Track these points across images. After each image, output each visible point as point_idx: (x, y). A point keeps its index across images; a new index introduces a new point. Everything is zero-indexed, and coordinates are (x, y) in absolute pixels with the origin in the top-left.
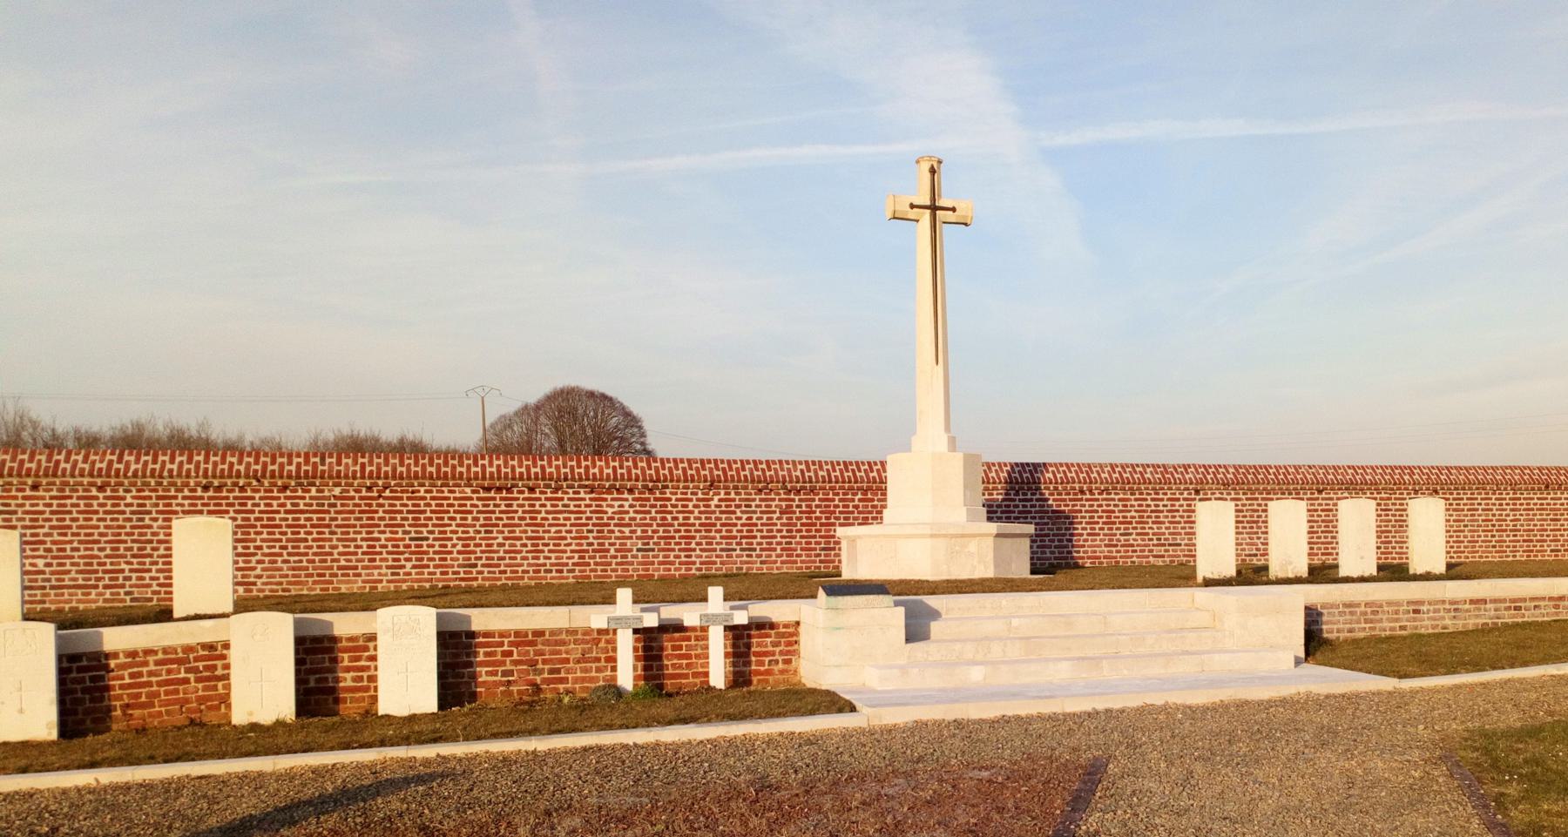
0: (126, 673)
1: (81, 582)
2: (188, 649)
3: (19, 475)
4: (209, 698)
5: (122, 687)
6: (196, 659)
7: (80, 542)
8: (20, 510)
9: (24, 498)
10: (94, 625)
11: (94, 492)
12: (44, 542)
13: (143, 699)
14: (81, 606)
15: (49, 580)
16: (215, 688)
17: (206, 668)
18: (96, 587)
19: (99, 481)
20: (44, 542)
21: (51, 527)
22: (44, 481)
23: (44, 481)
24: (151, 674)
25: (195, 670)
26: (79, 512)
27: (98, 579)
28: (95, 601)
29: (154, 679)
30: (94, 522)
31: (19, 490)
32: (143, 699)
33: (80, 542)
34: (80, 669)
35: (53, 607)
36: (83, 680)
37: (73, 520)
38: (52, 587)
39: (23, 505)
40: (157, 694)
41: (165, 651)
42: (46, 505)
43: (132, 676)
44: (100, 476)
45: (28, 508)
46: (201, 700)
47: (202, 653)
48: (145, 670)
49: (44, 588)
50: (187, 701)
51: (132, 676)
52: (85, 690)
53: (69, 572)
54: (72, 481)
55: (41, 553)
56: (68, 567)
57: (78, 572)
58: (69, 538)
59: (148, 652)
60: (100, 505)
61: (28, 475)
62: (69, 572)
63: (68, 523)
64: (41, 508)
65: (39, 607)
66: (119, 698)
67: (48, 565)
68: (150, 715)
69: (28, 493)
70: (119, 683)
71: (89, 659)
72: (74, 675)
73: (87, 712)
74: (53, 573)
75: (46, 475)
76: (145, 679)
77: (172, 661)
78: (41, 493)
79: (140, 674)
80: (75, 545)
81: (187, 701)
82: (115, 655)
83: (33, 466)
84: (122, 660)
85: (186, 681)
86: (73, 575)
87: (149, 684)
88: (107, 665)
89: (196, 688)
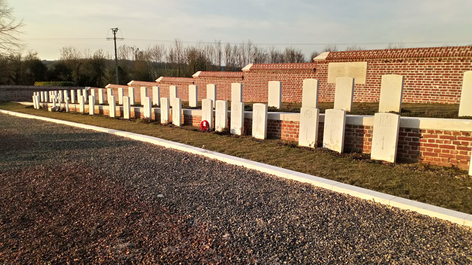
0: (427, 139)
1: (450, 94)
2: (456, 133)
3: (435, 56)
4: (462, 158)
5: (425, 145)
6: (459, 138)
7: (452, 80)
8: (434, 68)
9: (436, 64)
10: (416, 115)
11: (460, 62)
12: (440, 80)
13: (433, 152)
14: (449, 103)
15: (439, 93)
16: (466, 153)
17: (463, 143)
18: (455, 96)
19: (462, 58)
20: (440, 80)
21: (443, 75)
22: (443, 58)
23: (443, 58)
24: (438, 141)
25: (458, 143)
26: (453, 69)
27: (456, 94)
28: (454, 101)
29: (439, 144)
30: (458, 73)
31: (434, 62)
32: (433, 152)
33: (452, 80)
34: (410, 135)
35: (440, 102)
36: (410, 139)
37: (451, 72)
38: (440, 95)
39: (435, 67)
40: (439, 151)
41: (445, 132)
42: (442, 67)
43: (430, 141)
44: (462, 56)
45: (436, 68)
46: (459, 157)
47: (462, 136)
48: (435, 139)
49: (438, 95)
50: (452, 157)
51: (430, 141)
52: (410, 144)
53: (446, 90)
54: (452, 58)
55: (438, 83)
56: (447, 89)
57: (449, 91)
58: (448, 78)
59: (438, 132)
60: (461, 67)
61: (438, 56)
62: (446, 90)
63: (449, 73)
64: (441, 68)
65: (435, 102)
66: (423, 149)
67: (440, 87)
68: (435, 159)
69: (437, 62)
70: (424, 142)
71: (413, 131)
72: (407, 136)
73: (410, 153)
74: (441, 90)
75: (444, 56)
76: (435, 143)
77: (448, 138)
78: (442, 62)
79: (433, 141)
80: (450, 81)
81: (452, 157)
82: (424, 131)
83: (440, 53)
84: (427, 133)
85: (453, 147)
86: (448, 91)
87: (436, 146)
88: (420, 135)
89: (457, 152)
